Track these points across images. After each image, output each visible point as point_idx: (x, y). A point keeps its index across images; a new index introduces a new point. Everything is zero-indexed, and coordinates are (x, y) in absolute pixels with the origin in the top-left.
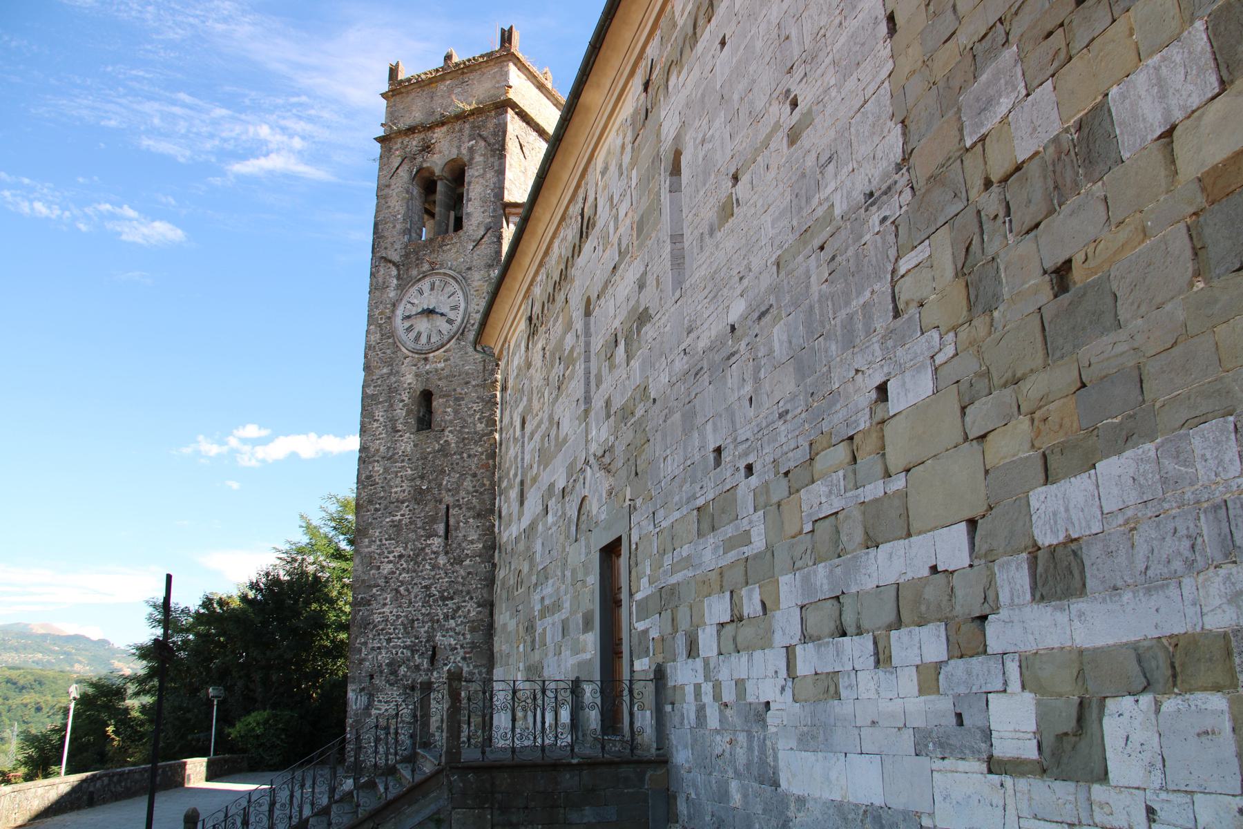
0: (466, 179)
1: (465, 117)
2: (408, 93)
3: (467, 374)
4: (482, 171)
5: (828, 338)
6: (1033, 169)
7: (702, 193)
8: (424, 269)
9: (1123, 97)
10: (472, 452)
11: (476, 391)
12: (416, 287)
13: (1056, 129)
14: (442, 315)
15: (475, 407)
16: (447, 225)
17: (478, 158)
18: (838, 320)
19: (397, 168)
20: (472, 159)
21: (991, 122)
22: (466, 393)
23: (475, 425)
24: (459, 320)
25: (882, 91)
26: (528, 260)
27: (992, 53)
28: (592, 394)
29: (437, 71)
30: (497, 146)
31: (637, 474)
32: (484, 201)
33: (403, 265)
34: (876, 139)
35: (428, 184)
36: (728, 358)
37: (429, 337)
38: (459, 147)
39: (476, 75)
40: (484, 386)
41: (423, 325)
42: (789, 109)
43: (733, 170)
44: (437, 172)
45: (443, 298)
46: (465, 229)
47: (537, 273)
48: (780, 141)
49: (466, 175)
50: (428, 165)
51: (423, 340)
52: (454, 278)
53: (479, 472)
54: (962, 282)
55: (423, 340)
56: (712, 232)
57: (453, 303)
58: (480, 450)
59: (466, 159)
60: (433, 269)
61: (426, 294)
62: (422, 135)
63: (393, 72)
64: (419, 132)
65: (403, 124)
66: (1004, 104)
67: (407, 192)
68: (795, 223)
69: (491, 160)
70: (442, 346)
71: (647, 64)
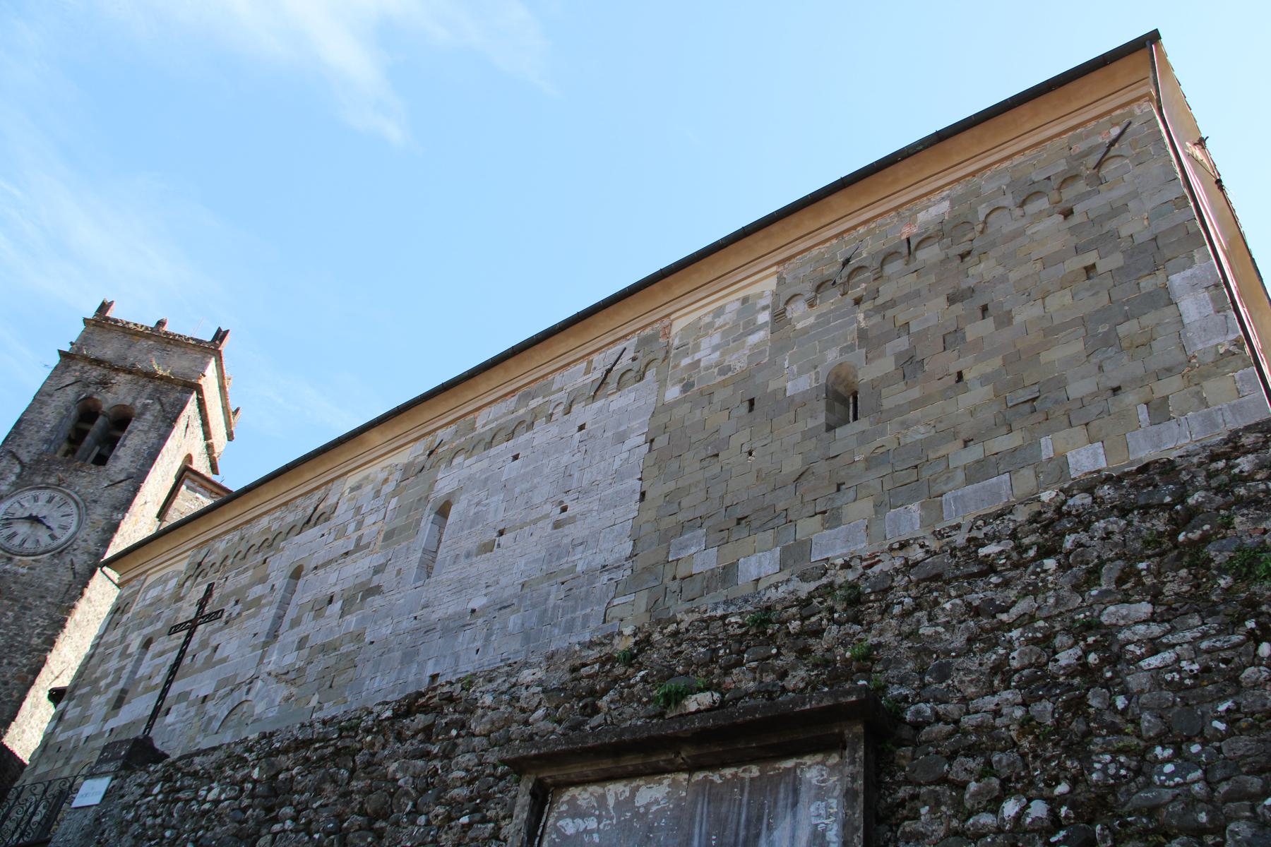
0: (129, 428)
1: (153, 378)
2: (109, 331)
3: (47, 589)
4: (146, 428)
5: (555, 625)
6: (699, 578)
7: (466, 532)
8: (49, 481)
9: (745, 563)
10: (14, 661)
11: (48, 608)
12: (33, 493)
13: (714, 565)
14: (49, 527)
15: (40, 621)
16: (89, 456)
17: (148, 416)
18: (564, 619)
19: (67, 386)
20: (142, 414)
21: (684, 554)
22: (36, 606)
23: (31, 637)
24: (63, 539)
25: (627, 523)
26: (222, 520)
27: (692, 528)
28: (281, 631)
29: (147, 328)
30: (170, 416)
31: (331, 687)
32: (137, 453)
33: (30, 468)
34: (616, 543)
35: (88, 412)
36: (464, 626)
37: (24, 542)
38: (135, 399)
39: (180, 351)
40: (58, 606)
41: (23, 529)
42: (559, 511)
43: (501, 528)
44: (105, 407)
45: (57, 514)
46: (107, 467)
47: (235, 528)
48: (547, 525)
49: (131, 424)
50: (99, 398)
51: (17, 541)
52: (77, 503)
53: (12, 682)
54: (649, 615)
55: (17, 541)
56: (468, 555)
57: (64, 521)
58: (25, 661)
59: (137, 411)
60: (59, 485)
61: (39, 503)
62: (105, 372)
63: (104, 307)
64: (105, 367)
65: (95, 353)
66: (693, 550)
67: (67, 410)
68: (544, 567)
69: (159, 423)
70: (34, 554)
71: (435, 441)
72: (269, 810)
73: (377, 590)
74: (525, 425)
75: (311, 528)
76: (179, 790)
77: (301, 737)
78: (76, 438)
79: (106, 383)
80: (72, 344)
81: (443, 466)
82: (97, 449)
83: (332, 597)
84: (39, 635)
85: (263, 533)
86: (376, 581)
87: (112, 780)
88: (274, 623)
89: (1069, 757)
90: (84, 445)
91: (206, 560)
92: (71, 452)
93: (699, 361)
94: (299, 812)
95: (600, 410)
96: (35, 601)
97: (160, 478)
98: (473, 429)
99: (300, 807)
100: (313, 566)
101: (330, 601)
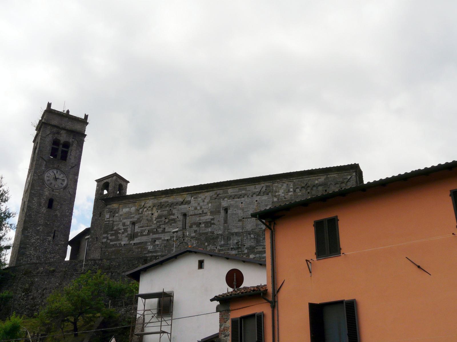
63: (49, 105)
78: (54, 152)
86: (212, 222)
89: (106, 242)
93: (280, 195)
96: (63, 202)
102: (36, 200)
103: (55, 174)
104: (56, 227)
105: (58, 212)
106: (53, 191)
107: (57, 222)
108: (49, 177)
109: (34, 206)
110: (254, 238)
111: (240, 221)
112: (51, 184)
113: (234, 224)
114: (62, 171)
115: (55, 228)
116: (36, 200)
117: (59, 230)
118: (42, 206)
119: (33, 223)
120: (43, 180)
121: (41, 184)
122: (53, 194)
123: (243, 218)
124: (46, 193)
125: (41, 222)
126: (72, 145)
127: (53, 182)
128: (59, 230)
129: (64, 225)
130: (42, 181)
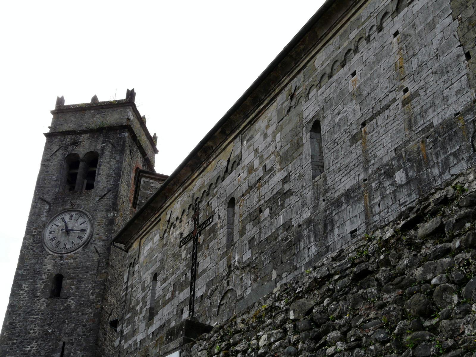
3: (87, 267)
4: (108, 160)
16: (82, 186)
20: (103, 153)
22: (85, 278)
23: (88, 296)
25: (463, 79)
32: (108, 176)
33: (53, 204)
38: (96, 146)
46: (95, 189)
49: (99, 160)
55: (62, 246)
58: (90, 311)
59: (99, 152)
65: (66, 127)
72: (317, 338)
73: (290, 193)
74: (352, 51)
75: (230, 174)
76: (235, 344)
77: (319, 276)
79: (77, 143)
80: (49, 127)
81: (303, 103)
82: (86, 181)
83: (260, 209)
84: (92, 294)
85: (201, 187)
86: (286, 187)
87: (181, 353)
88: (228, 239)
90: (77, 181)
91: (172, 218)
92: (72, 189)
94: (345, 334)
95: (406, 16)
97: (126, 186)
98: (316, 70)
99: (344, 329)
100: (240, 195)
101: (261, 211)
102: (27, 287)
103: (65, 222)
104: (67, 333)
105: (71, 299)
106: (62, 257)
107: (67, 324)
108: (54, 232)
109: (22, 302)
110: (409, 181)
111: (354, 139)
112: (58, 244)
113: (338, 165)
114: (81, 212)
115: (65, 339)
116: (27, 287)
117: (72, 340)
118: (38, 297)
119: (17, 340)
120: (42, 241)
121: (37, 251)
122: (62, 264)
123: (364, 124)
124: (48, 266)
125: (35, 333)
126: (102, 156)
127: (62, 239)
128: (72, 340)
129: (85, 326)
130: (39, 244)
